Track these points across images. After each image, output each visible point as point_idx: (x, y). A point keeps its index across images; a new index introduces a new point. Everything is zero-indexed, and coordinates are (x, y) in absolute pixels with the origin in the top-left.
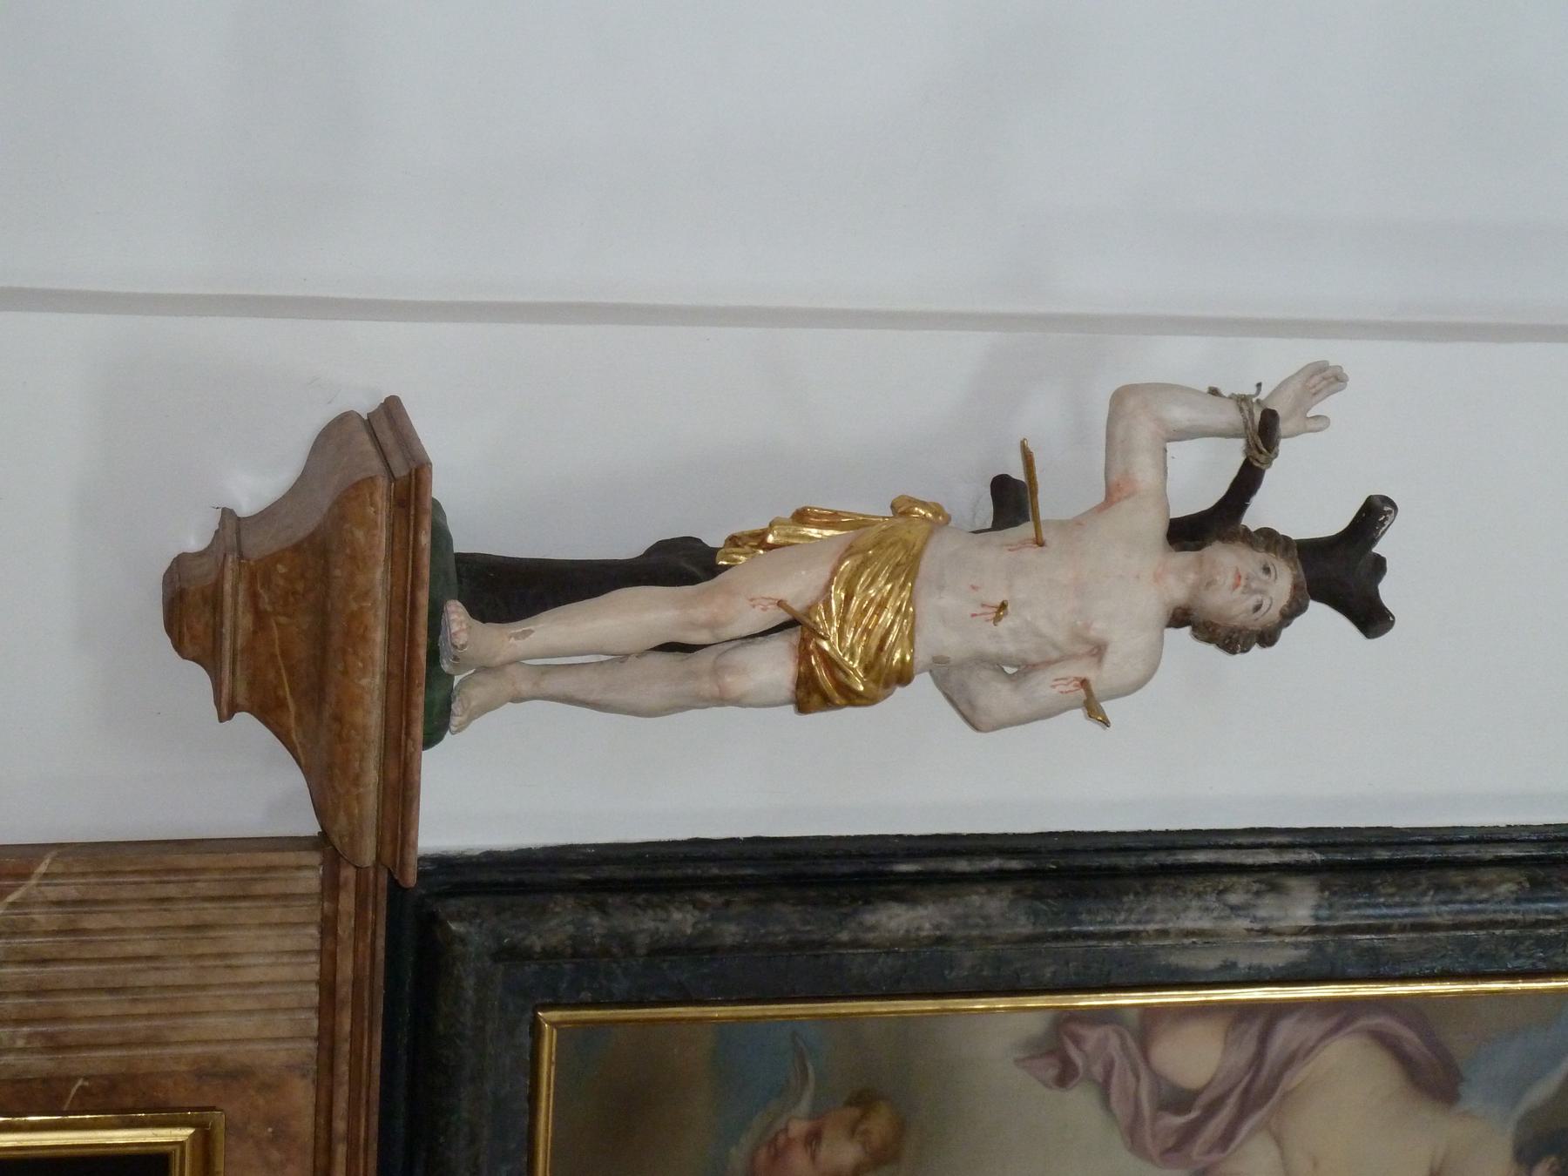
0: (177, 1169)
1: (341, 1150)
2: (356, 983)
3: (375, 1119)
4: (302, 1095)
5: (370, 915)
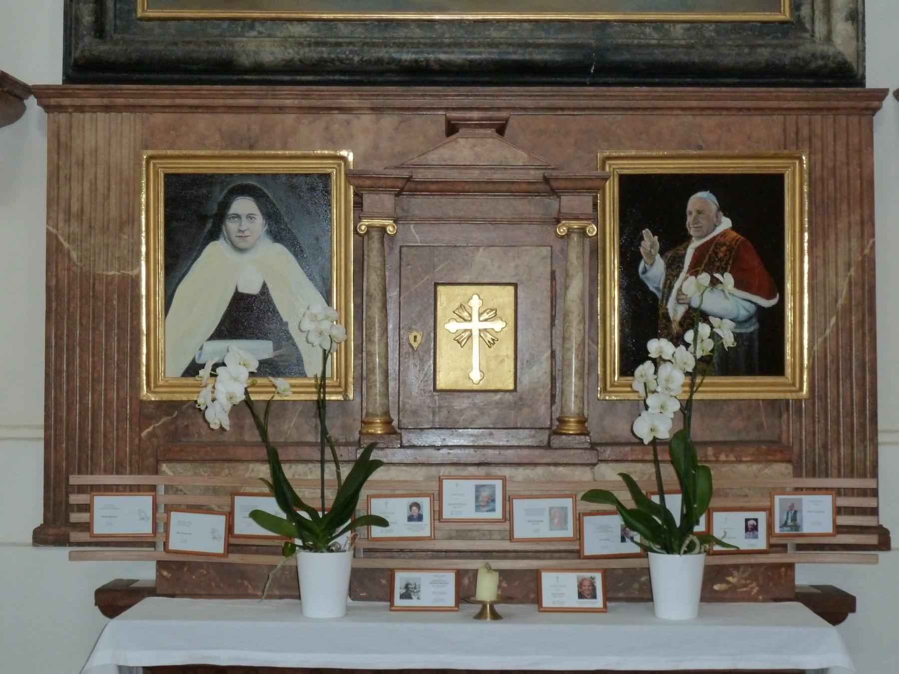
0: (616, 247)
1: (178, 101)
2: (102, 96)
3: (162, 87)
4: (158, 118)
5: (70, 91)
